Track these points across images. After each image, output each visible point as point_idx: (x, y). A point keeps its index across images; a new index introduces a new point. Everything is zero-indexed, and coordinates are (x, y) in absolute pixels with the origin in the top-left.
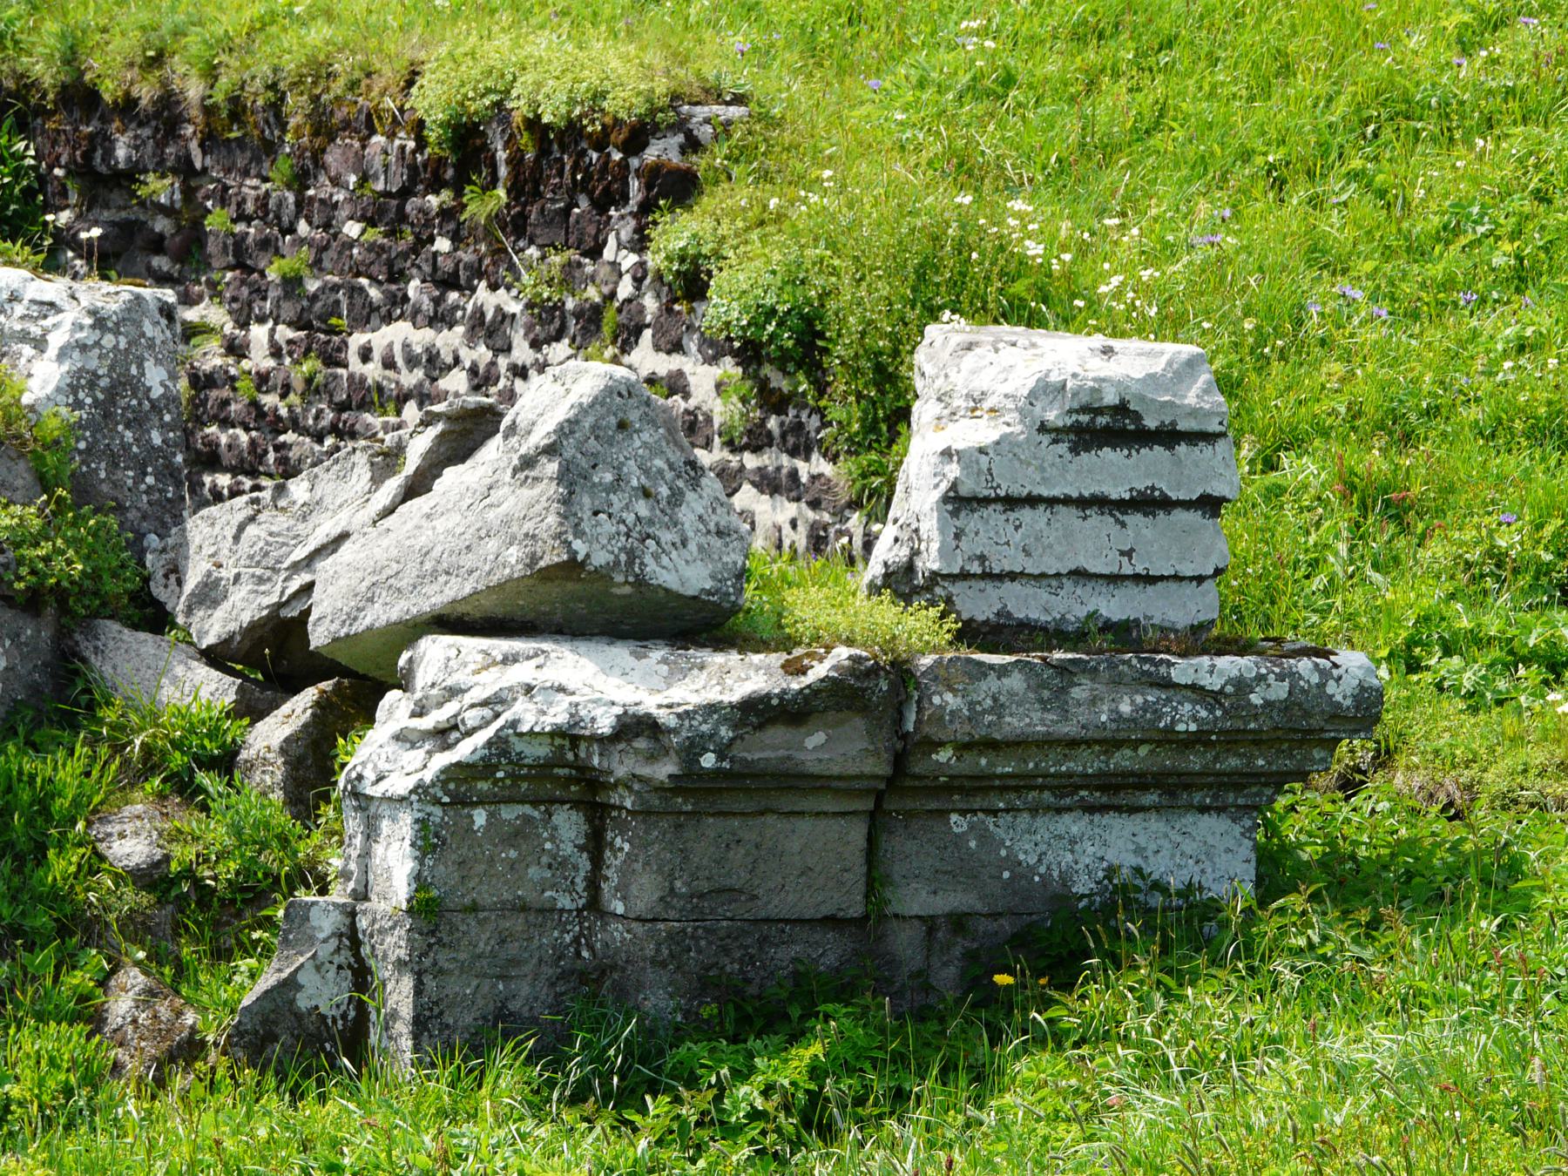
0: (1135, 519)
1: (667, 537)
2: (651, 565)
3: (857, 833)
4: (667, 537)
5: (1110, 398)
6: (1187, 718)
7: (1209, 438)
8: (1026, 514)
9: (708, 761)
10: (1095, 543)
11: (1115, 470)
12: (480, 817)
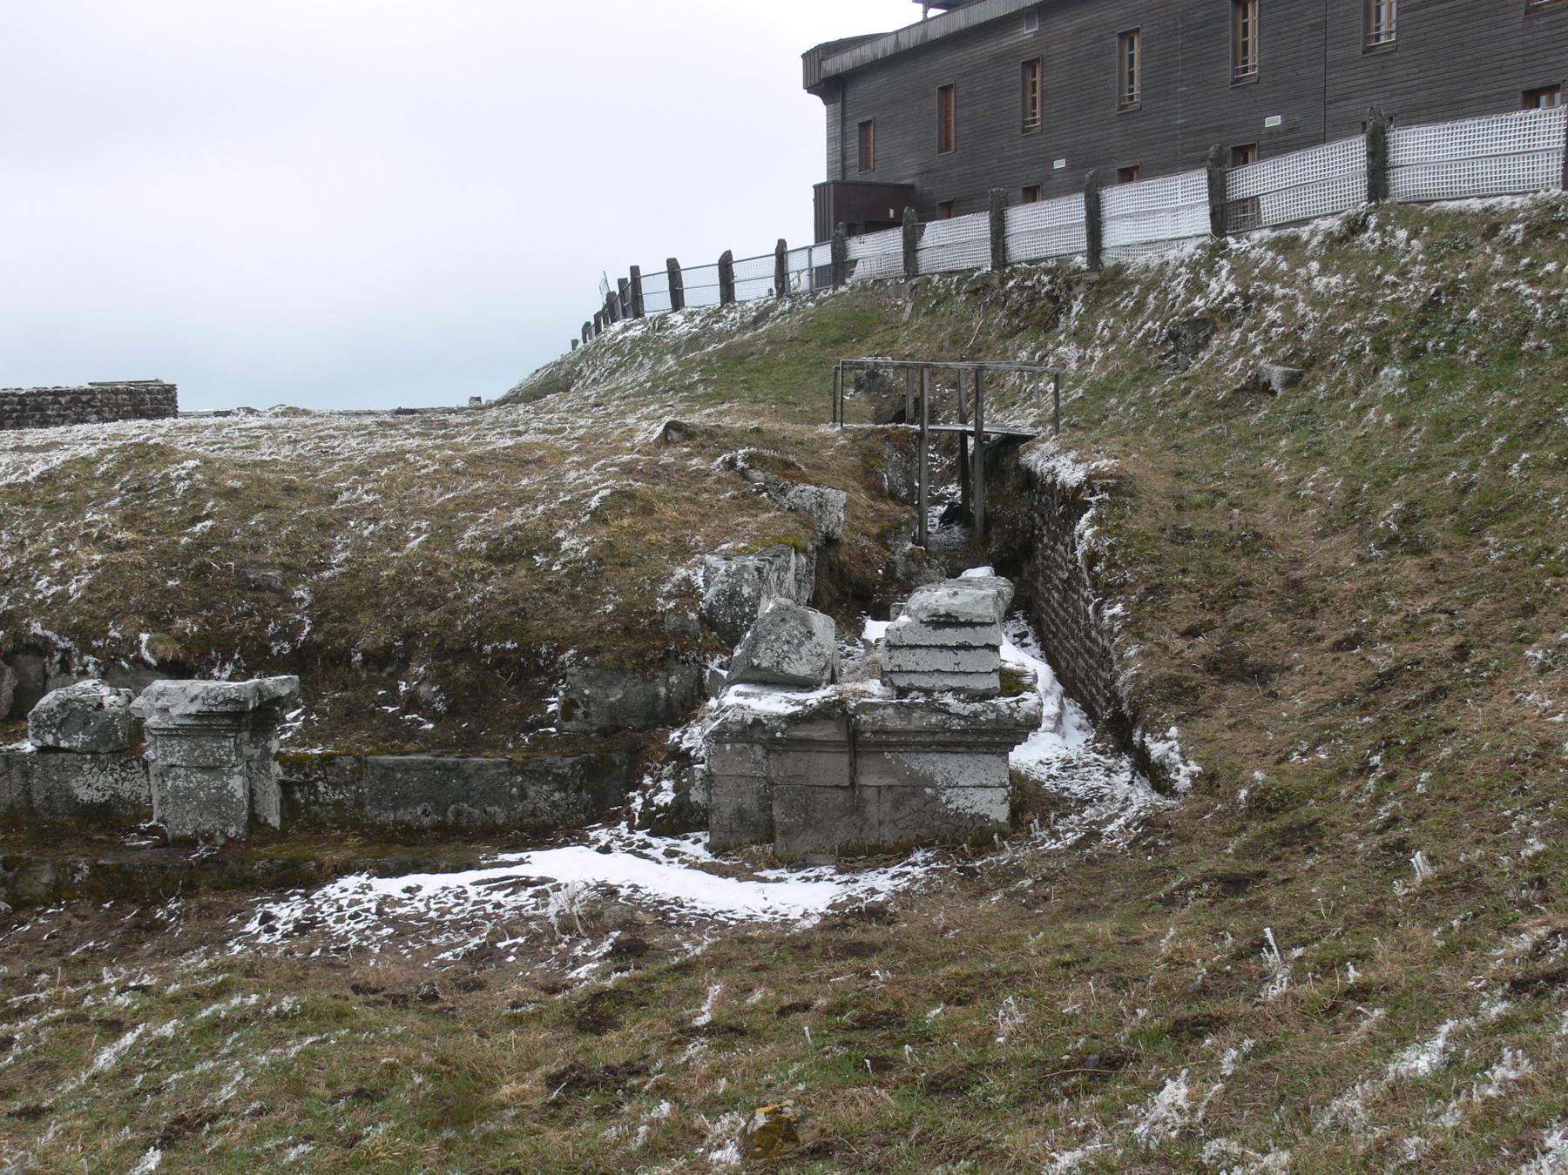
0: (962, 653)
1: (793, 657)
2: (785, 666)
3: (845, 759)
4: (793, 657)
5: (942, 611)
6: (956, 724)
7: (989, 624)
8: (918, 651)
9: (778, 735)
10: (945, 661)
11: (950, 636)
12: (728, 747)
